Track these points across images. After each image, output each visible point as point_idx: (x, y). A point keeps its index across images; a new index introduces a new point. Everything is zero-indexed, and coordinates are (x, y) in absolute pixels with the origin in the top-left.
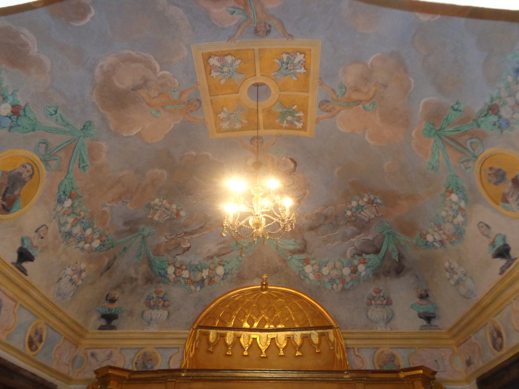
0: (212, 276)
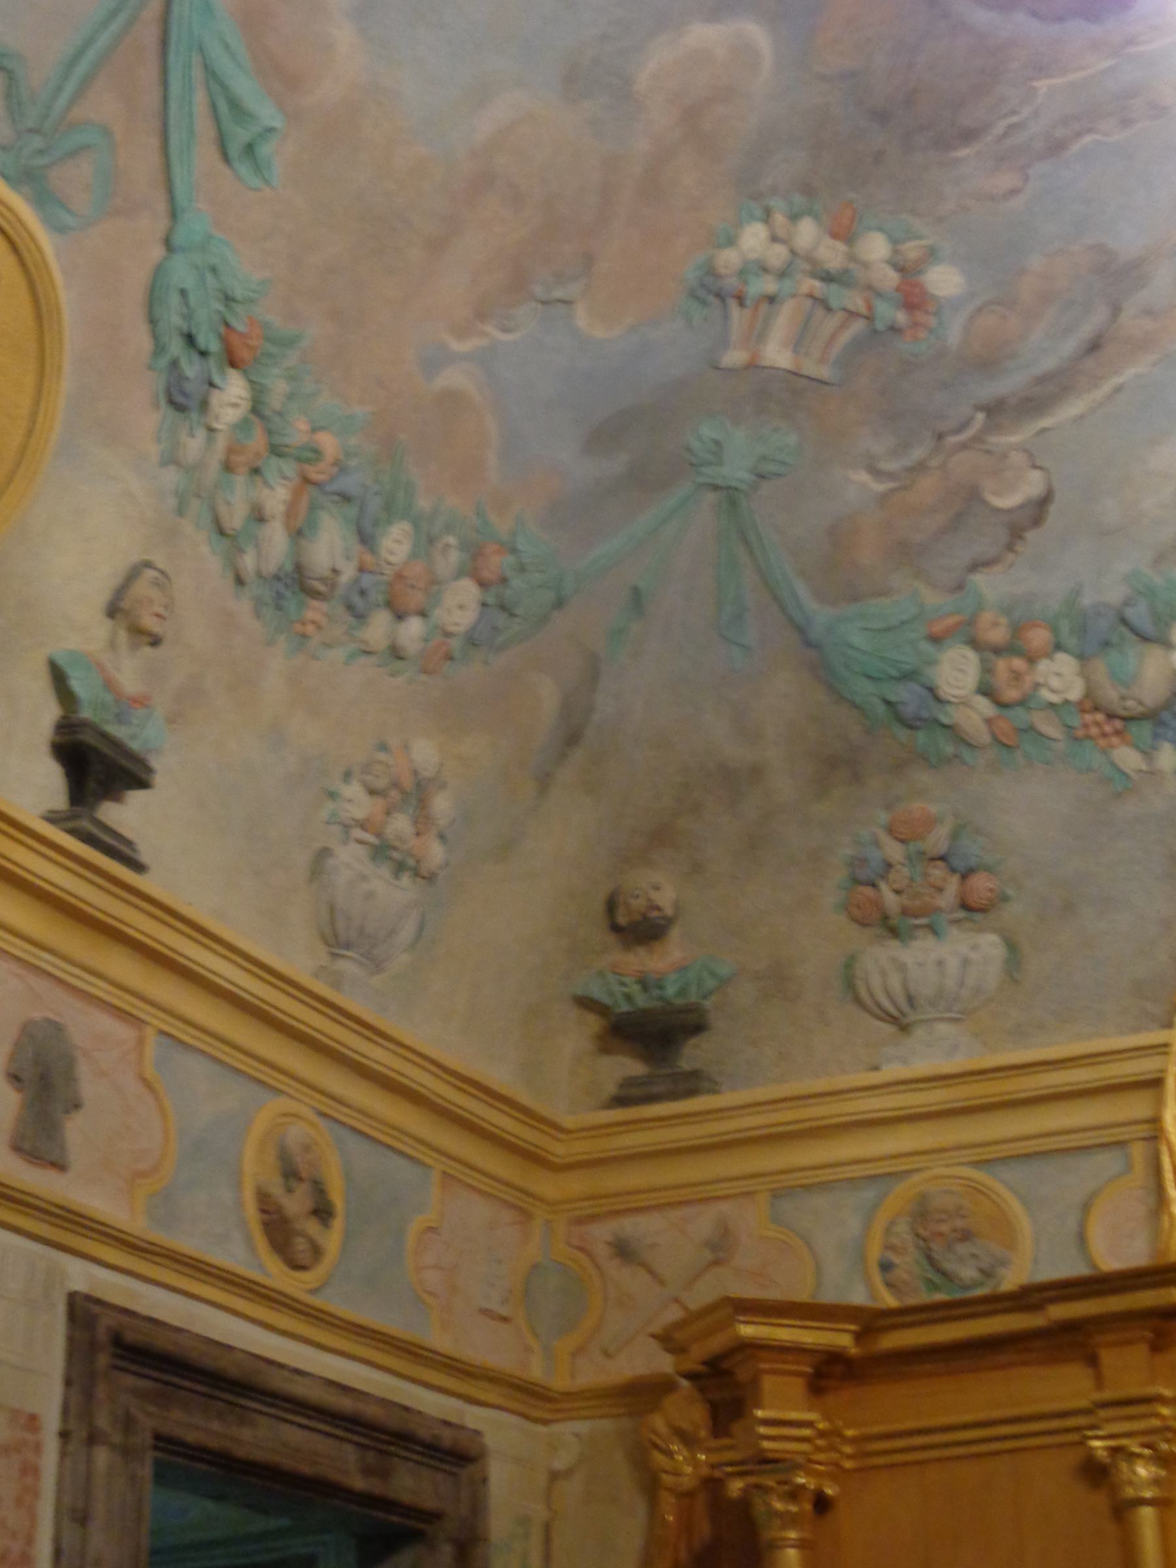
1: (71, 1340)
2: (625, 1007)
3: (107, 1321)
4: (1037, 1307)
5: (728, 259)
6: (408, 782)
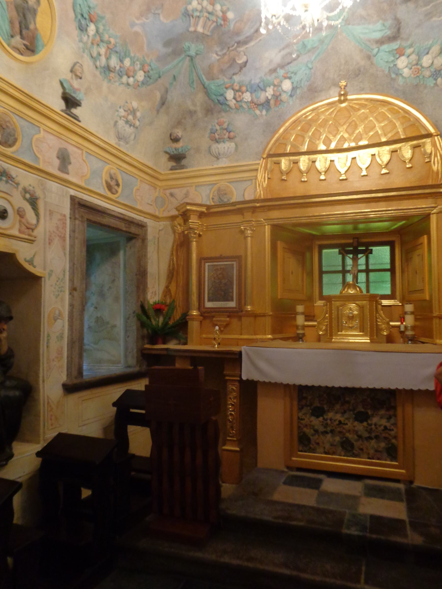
0: (278, 94)
2: (172, 153)
3: (77, 200)
5: (190, 8)
6: (132, 109)
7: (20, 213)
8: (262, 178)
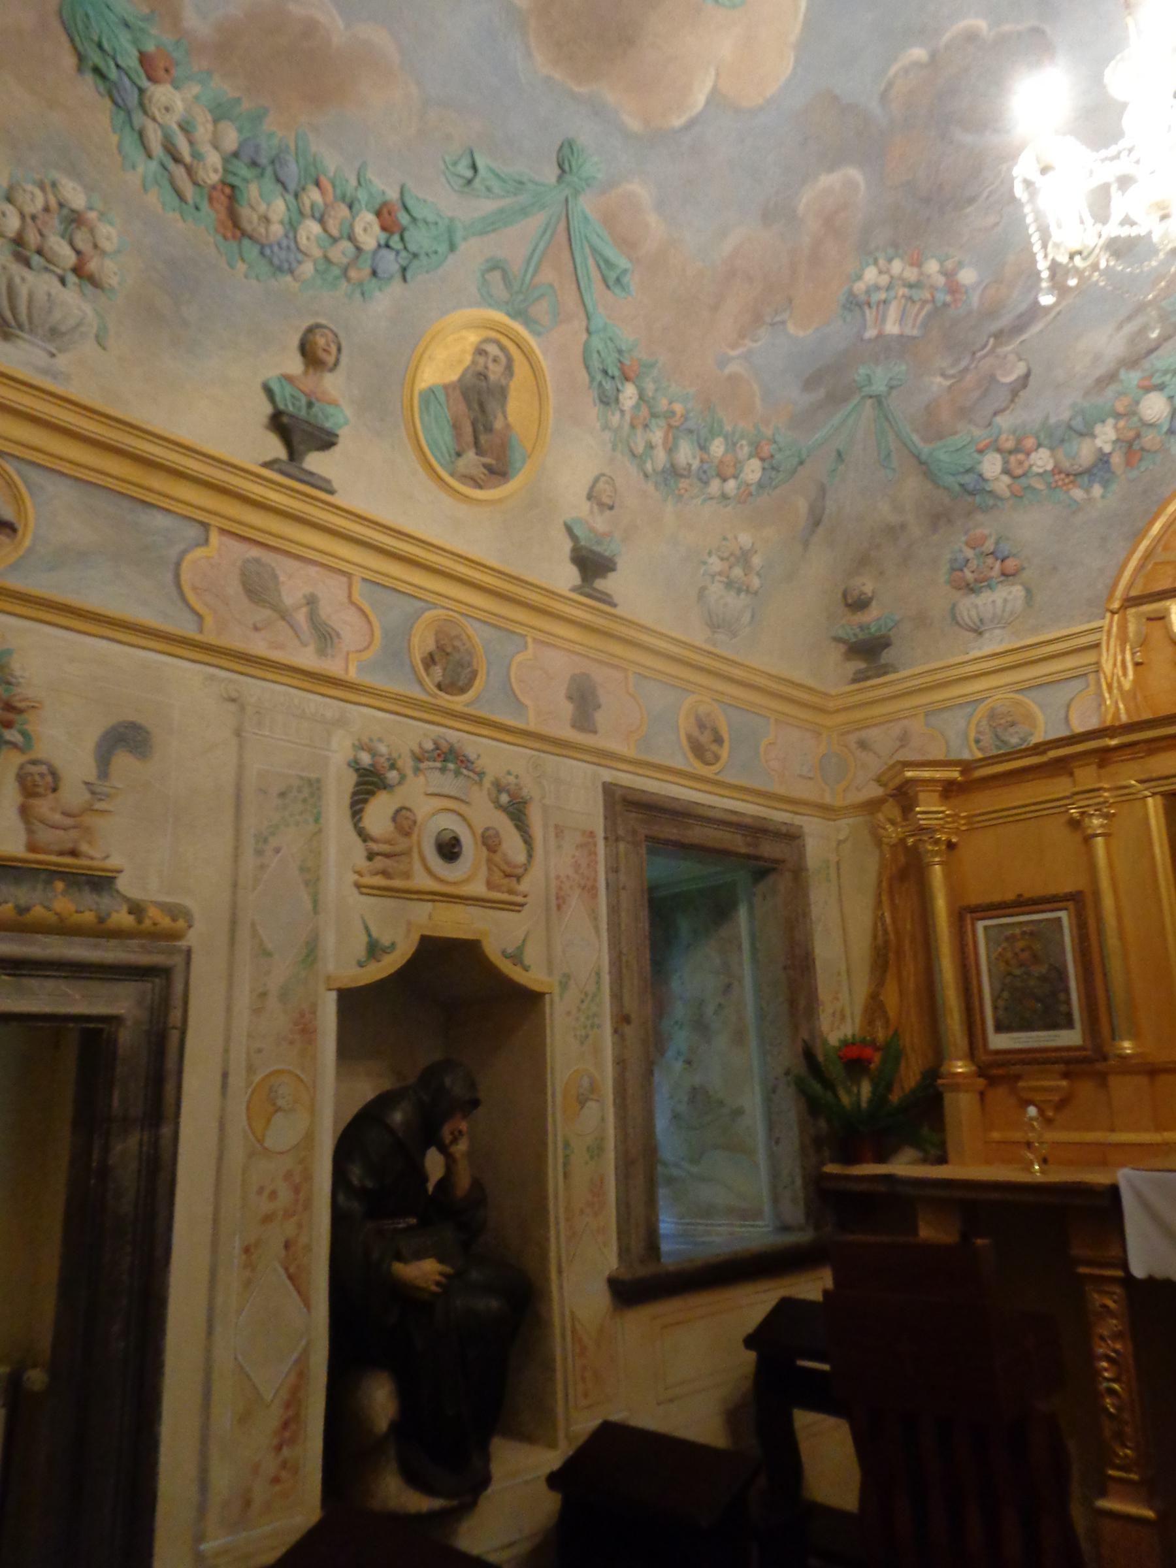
0: (1131, 434)
1: (605, 800)
2: (854, 640)
3: (619, 792)
4: (1044, 752)
5: (859, 287)
6: (738, 553)
7: (490, 842)
8: (1115, 665)
